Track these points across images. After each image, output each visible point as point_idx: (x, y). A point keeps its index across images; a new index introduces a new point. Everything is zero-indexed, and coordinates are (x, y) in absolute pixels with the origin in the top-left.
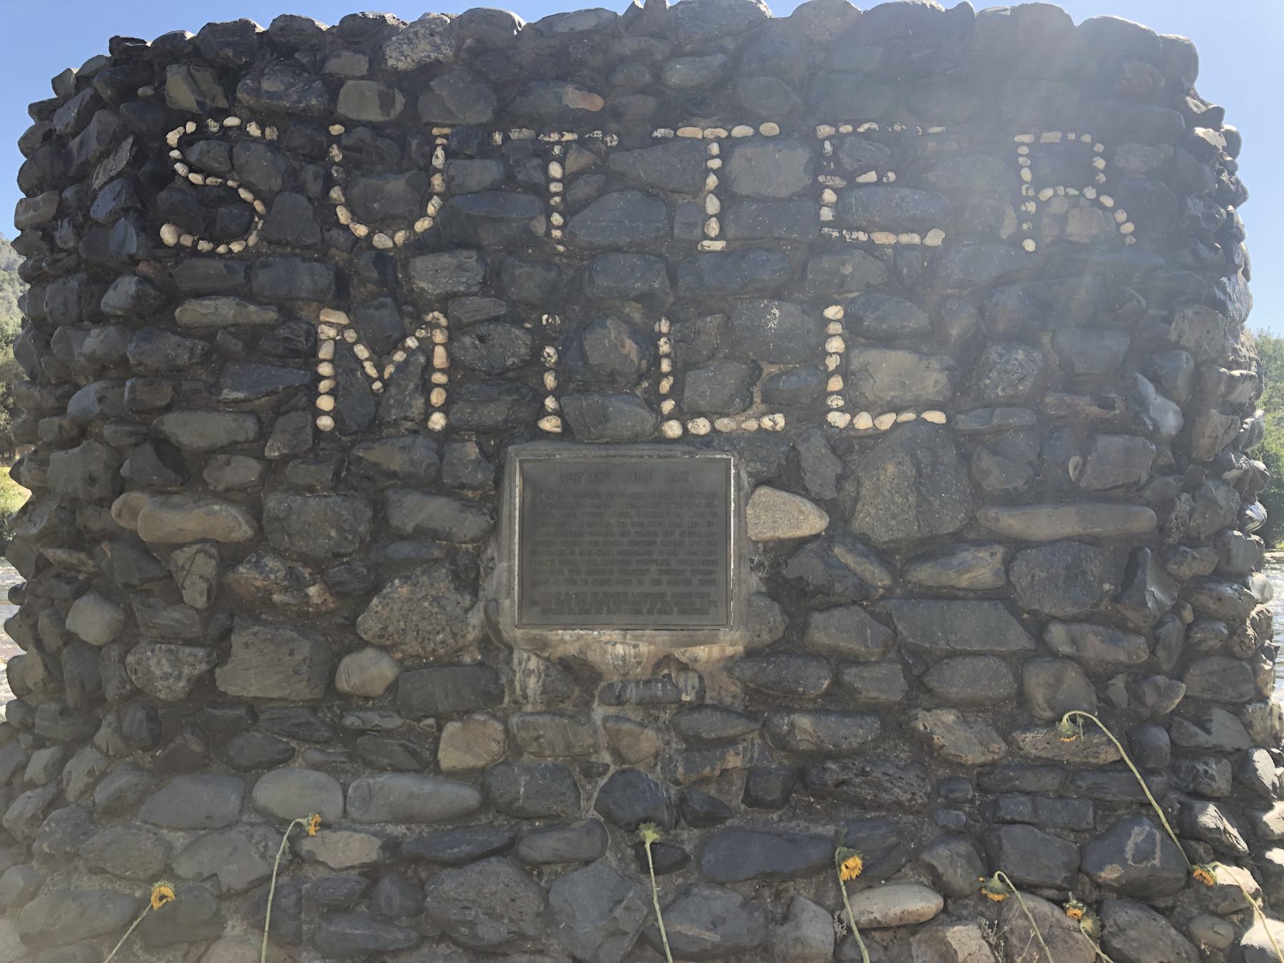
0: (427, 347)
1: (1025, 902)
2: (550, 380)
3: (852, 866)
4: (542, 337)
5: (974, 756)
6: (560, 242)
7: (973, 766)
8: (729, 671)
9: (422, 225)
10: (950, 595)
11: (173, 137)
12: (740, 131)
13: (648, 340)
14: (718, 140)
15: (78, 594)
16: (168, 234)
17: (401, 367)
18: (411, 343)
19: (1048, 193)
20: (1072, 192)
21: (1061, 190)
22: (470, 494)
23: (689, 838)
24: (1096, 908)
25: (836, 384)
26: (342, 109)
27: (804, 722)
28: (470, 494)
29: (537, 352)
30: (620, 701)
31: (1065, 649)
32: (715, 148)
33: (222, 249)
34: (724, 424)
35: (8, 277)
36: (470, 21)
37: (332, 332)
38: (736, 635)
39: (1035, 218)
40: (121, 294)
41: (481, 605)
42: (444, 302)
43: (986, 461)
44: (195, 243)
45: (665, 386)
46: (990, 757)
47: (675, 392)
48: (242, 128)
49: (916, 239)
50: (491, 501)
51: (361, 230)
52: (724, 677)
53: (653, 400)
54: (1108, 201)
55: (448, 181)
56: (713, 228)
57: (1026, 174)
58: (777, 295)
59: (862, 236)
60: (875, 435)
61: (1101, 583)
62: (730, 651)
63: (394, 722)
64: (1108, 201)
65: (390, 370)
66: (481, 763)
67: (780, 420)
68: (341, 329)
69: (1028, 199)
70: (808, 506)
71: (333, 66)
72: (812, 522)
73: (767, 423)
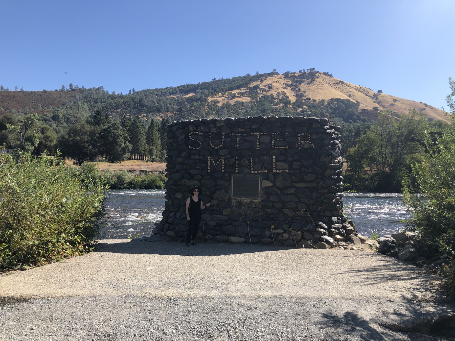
0: (221, 161)
1: (293, 231)
2: (237, 166)
3: (273, 227)
4: (236, 160)
5: (291, 215)
6: (238, 148)
7: (290, 216)
8: (150, 152)
9: (221, 146)
10: (289, 194)
11: (190, 134)
12: (262, 134)
13: (249, 160)
14: (259, 135)
15: (177, 192)
16: (189, 147)
17: (218, 164)
18: (220, 161)
19: (302, 142)
20: (305, 141)
21: (304, 141)
22: (227, 180)
23: (253, 224)
24: (302, 233)
25: (274, 166)
26: (211, 131)
27: (269, 210)
28: (227, 180)
29: (235, 162)
30: (245, 207)
31: (303, 201)
32: (258, 136)
33: (196, 149)
34: (259, 172)
35: (85, 100)
36: (234, 81)
37: (210, 159)
38: (260, 199)
39: (300, 145)
40: (184, 154)
41: (228, 195)
42: (224, 156)
43: (293, 177)
44: (193, 148)
45: (252, 166)
46: (292, 215)
47: (253, 167)
48: (198, 133)
49: (285, 148)
51: (213, 147)
52: (156, 152)
53: (250, 168)
54: (310, 143)
55: (224, 140)
56: (258, 146)
57: (299, 139)
58: (266, 155)
59: (277, 147)
60: (279, 173)
61: (308, 193)
62: (259, 201)
63: (217, 209)
64: (310, 143)
65: (217, 164)
66: (228, 214)
67: (267, 171)
68: (211, 159)
69: (299, 142)
70: (270, 182)
71: (210, 126)
72: (270, 184)
73: (265, 171)
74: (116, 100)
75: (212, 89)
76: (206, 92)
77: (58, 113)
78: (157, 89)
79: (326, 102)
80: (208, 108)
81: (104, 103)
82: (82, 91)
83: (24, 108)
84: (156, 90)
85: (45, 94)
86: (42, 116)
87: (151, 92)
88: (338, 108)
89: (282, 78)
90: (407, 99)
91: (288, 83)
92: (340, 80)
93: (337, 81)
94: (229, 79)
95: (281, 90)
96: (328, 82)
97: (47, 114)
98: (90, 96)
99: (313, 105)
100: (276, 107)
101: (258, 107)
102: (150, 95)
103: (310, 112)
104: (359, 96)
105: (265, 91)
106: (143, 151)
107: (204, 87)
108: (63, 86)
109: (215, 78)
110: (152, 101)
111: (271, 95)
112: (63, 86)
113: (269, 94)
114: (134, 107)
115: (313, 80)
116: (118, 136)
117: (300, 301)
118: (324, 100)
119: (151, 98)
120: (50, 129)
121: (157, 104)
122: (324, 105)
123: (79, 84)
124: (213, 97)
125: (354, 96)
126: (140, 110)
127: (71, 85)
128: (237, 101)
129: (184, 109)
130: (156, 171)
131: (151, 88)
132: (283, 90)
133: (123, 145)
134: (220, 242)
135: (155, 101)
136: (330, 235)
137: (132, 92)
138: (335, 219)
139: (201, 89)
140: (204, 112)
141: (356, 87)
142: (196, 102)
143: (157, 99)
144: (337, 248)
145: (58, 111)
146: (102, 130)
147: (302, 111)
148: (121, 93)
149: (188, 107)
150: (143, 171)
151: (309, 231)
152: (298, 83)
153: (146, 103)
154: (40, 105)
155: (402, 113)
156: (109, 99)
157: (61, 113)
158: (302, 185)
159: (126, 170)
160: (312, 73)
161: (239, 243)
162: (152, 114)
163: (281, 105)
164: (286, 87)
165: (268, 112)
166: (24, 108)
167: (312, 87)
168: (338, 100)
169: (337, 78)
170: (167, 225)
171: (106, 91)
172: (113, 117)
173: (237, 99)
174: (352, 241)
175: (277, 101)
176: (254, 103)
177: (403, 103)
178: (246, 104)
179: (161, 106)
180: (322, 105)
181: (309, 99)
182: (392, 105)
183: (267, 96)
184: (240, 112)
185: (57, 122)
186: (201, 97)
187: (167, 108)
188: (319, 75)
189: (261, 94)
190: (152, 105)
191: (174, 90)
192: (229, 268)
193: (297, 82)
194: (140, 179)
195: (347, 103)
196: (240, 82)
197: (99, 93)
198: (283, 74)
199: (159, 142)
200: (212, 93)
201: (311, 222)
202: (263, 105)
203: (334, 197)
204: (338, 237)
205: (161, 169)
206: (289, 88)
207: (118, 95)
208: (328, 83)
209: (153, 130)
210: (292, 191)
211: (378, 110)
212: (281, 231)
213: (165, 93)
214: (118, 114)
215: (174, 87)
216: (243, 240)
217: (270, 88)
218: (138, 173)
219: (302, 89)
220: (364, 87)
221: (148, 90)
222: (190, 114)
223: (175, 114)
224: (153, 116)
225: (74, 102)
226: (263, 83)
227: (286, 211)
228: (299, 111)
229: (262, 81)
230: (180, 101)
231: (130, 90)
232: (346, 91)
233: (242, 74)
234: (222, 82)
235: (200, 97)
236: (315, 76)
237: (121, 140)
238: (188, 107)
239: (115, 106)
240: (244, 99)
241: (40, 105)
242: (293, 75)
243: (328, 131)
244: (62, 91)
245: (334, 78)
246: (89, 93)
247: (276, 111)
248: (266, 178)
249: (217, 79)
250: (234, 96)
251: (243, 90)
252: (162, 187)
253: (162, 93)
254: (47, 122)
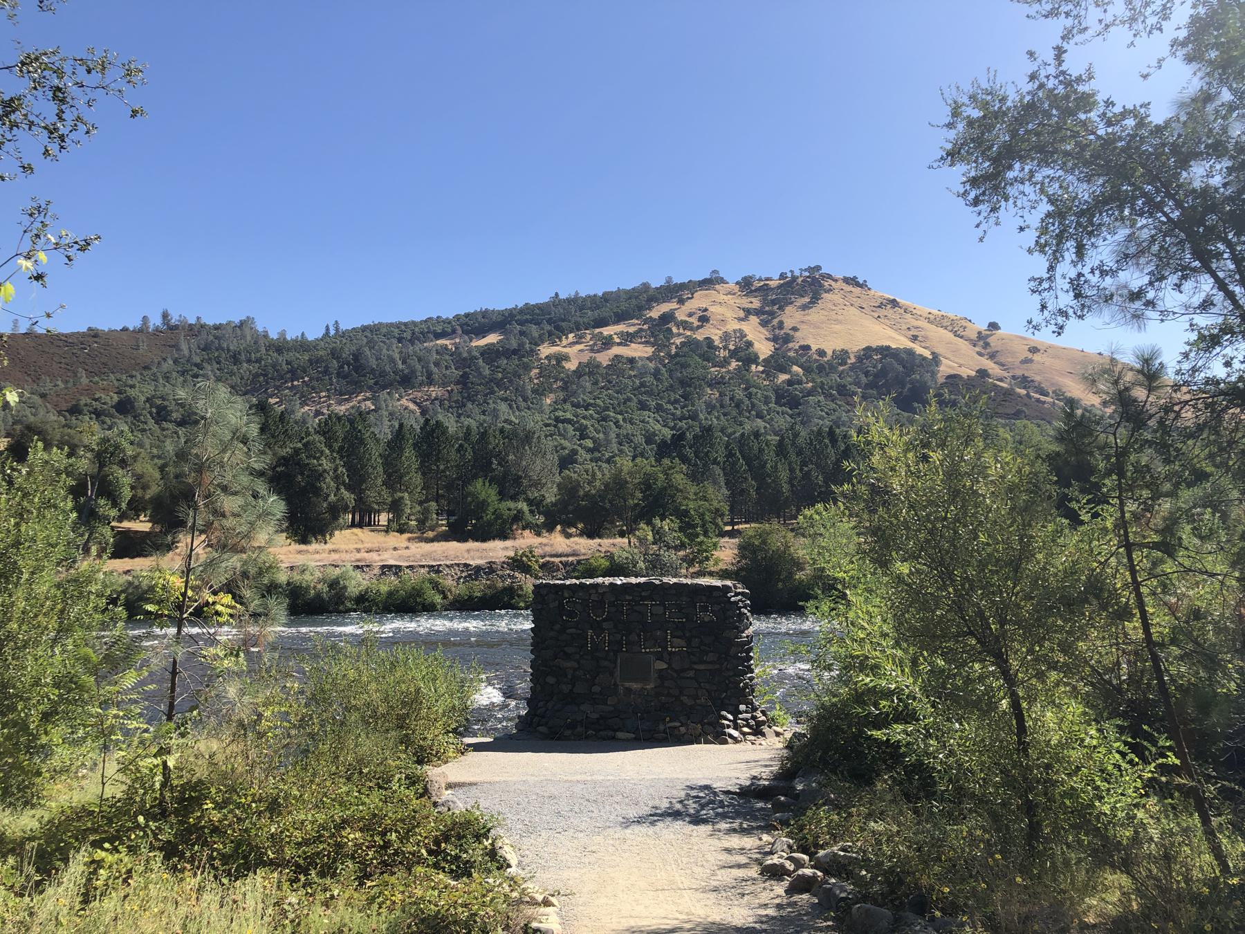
3: (668, 719)
4: (623, 635)
13: (639, 636)
36: (606, 301)
40: (557, 627)
50: (615, 663)
72: (665, 666)
74: (291, 356)
75: (549, 322)
76: (534, 330)
77: (132, 393)
78: (400, 323)
79: (852, 356)
80: (540, 375)
81: (256, 362)
82: (195, 330)
83: (37, 380)
84: (398, 325)
85: (96, 339)
86: (89, 401)
87: (384, 330)
88: (883, 373)
89: (734, 294)
90: (1064, 346)
91: (750, 306)
92: (887, 296)
93: (880, 301)
94: (595, 296)
95: (733, 326)
96: (858, 302)
97: (103, 396)
98: (219, 344)
99: (819, 366)
100: (719, 372)
101: (671, 371)
102: (384, 342)
103: (810, 385)
104: (940, 339)
105: (691, 329)
106: (377, 503)
107: (528, 317)
108: (145, 319)
109: (557, 294)
110: (389, 356)
111: (707, 338)
112: (145, 319)
113: (700, 336)
114: (338, 375)
115: (815, 299)
116: (321, 475)
117: (672, 780)
118: (847, 352)
119: (385, 351)
120: (142, 455)
121: (401, 366)
122: (846, 364)
123: (188, 311)
124: (553, 344)
125: (926, 338)
126: (356, 383)
127: (165, 316)
128: (616, 356)
129: (474, 377)
130: (423, 566)
131: (384, 321)
132: (736, 325)
133: (332, 498)
134: (604, 739)
135: (397, 356)
136: (736, 728)
137: (332, 332)
138: (742, 707)
139: (521, 323)
140: (529, 387)
142: (507, 358)
143: (401, 352)
144: (743, 743)
145: (132, 387)
146: (279, 460)
147: (790, 383)
148: (303, 334)
149: (487, 372)
150: (390, 567)
151: (710, 724)
152: (777, 306)
153: (373, 363)
154: (82, 373)
155: (1052, 384)
156: (271, 353)
157: (140, 393)
158: (702, 667)
159: (349, 567)
160: (814, 279)
161: (628, 740)
162: (388, 393)
163: (734, 364)
164: (746, 317)
165: (700, 385)
166: (37, 380)
167: (814, 315)
168: (885, 351)
169: (881, 291)
170: (536, 719)
171: (260, 329)
172: (281, 401)
173: (616, 350)
174: (763, 735)
175: (723, 353)
176: (661, 361)
177: (1055, 357)
178: (640, 363)
179: (413, 372)
180: (841, 364)
181: (807, 348)
182: (1026, 361)
183: (697, 342)
184: (626, 386)
185: (130, 419)
186: (521, 345)
187: (429, 375)
188: (833, 283)
189: (679, 335)
190: (388, 368)
191: (446, 325)
192: (619, 763)
193: (773, 302)
194: (384, 589)
195: (907, 360)
196: (624, 306)
197: (243, 337)
198: (737, 283)
199: (417, 479)
200: (550, 334)
201: (713, 713)
202: (684, 366)
203: (742, 681)
204: (746, 730)
205: (434, 560)
206: (754, 320)
207: (296, 341)
208: (857, 304)
209: (402, 450)
210: (691, 674)
211: (988, 376)
212: (677, 724)
213: (421, 333)
214: (295, 394)
215: (447, 319)
216: (633, 736)
217: (704, 319)
218: (377, 571)
219: (789, 323)
220: (951, 315)
221: (375, 325)
222: (493, 392)
223: (452, 390)
224: (392, 398)
225: (176, 361)
226: (683, 308)
227: (684, 699)
228: (780, 381)
229: (681, 301)
230: (465, 355)
232: (904, 327)
233: (629, 282)
234: (577, 303)
235: (519, 345)
236: (821, 286)
237: (328, 484)
238: (487, 372)
239: (288, 372)
240: (635, 350)
241: (82, 373)
242: (765, 285)
243: (733, 599)
244: (140, 331)
245: (872, 292)
246: (216, 338)
247: (719, 383)
248: (660, 657)
249: (562, 296)
250: (607, 343)
251: (634, 325)
252: (439, 607)
253: (413, 333)
254: (103, 417)
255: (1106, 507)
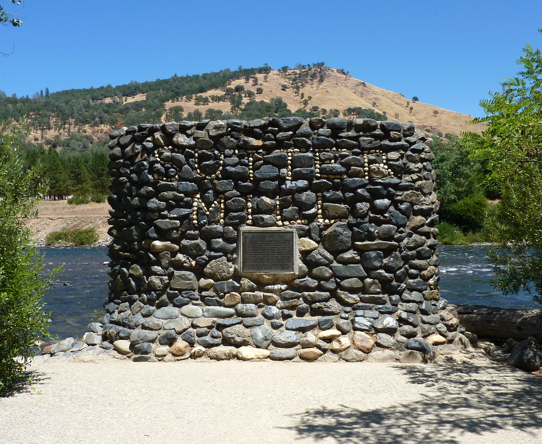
109: (176, 75)
118: (338, 111)
131: (75, 88)
141: (383, 92)
188: (331, 73)
231: (42, 91)
255: (274, 307)
